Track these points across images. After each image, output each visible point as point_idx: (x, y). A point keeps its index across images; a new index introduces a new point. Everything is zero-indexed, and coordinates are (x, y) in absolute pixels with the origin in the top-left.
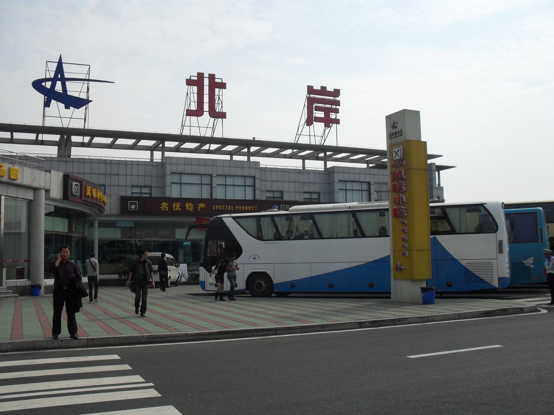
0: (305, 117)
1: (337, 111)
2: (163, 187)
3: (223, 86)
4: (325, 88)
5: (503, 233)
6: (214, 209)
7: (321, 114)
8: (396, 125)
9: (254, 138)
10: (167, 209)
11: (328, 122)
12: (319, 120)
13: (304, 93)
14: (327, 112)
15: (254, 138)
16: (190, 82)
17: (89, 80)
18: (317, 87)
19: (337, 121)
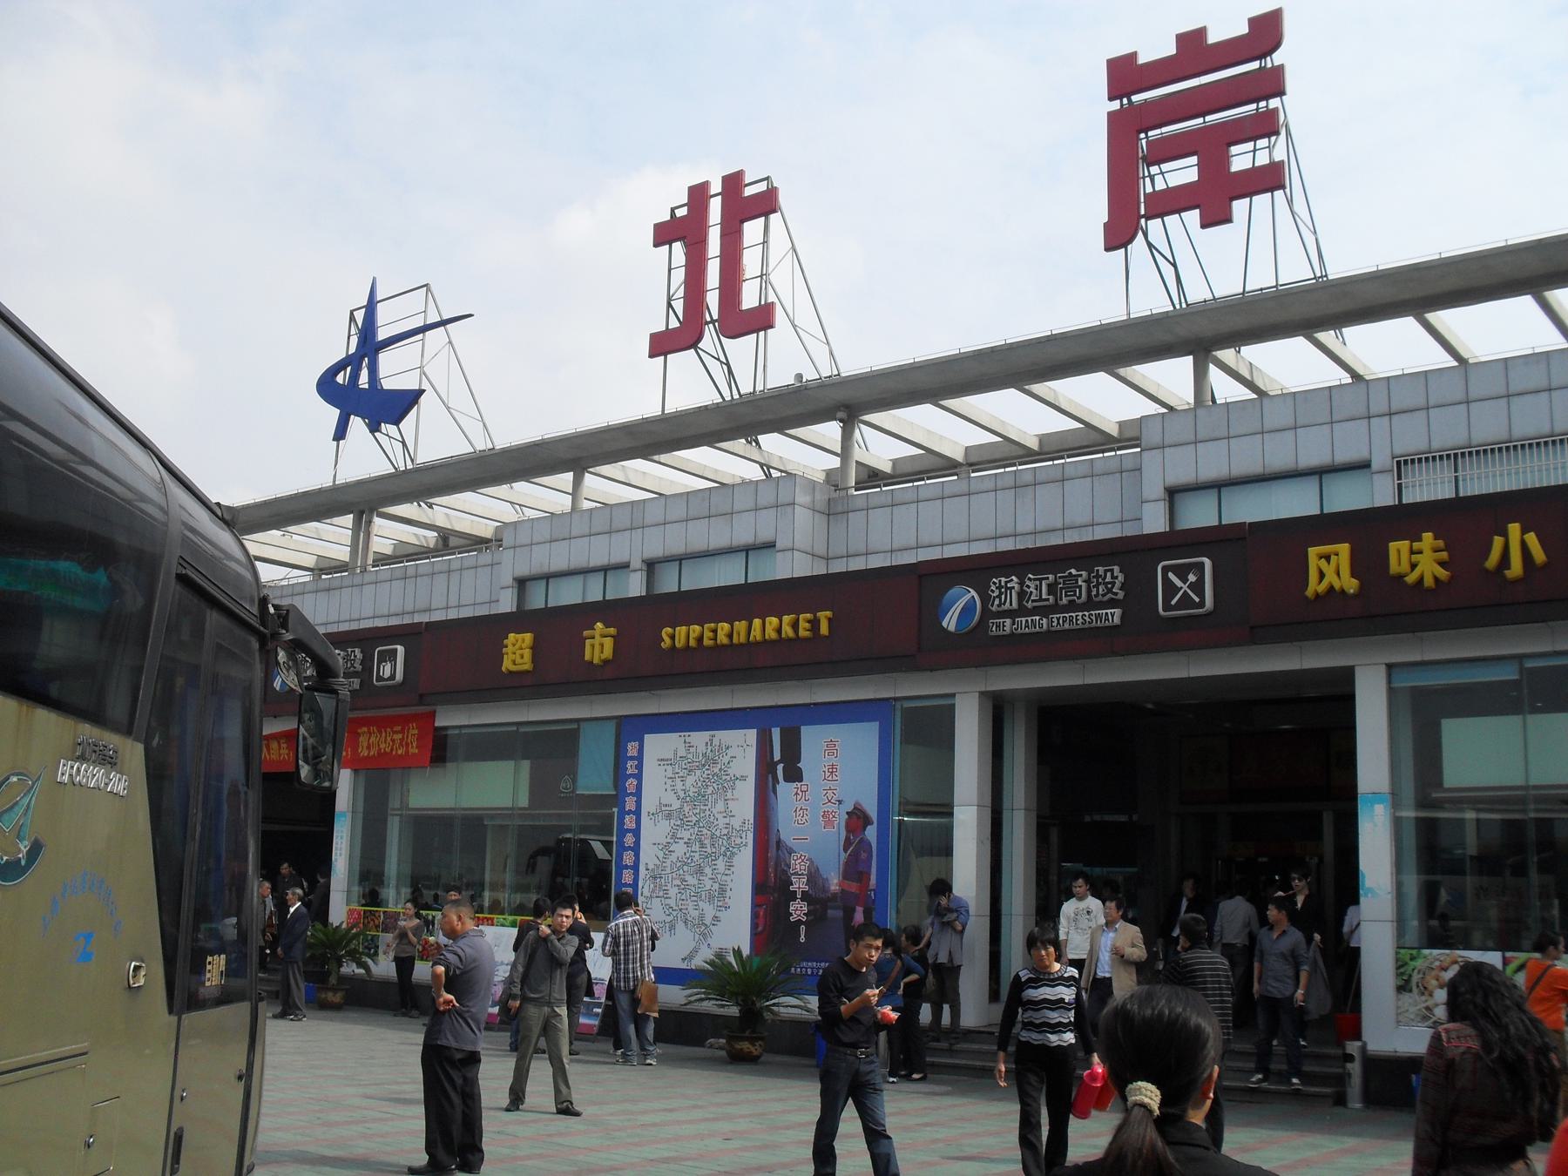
0: (1098, 209)
1: (1267, 126)
2: (747, 551)
3: (766, 204)
4: (1200, 33)
5: (1438, 878)
6: (666, 643)
7: (1183, 172)
8: (395, 370)
9: (799, 377)
10: (1313, 552)
11: (1214, 199)
12: (1170, 203)
13: (1096, 108)
14: (1211, 149)
15: (799, 377)
16: (664, 234)
17: (443, 323)
18: (1157, 46)
19: (1270, 179)
